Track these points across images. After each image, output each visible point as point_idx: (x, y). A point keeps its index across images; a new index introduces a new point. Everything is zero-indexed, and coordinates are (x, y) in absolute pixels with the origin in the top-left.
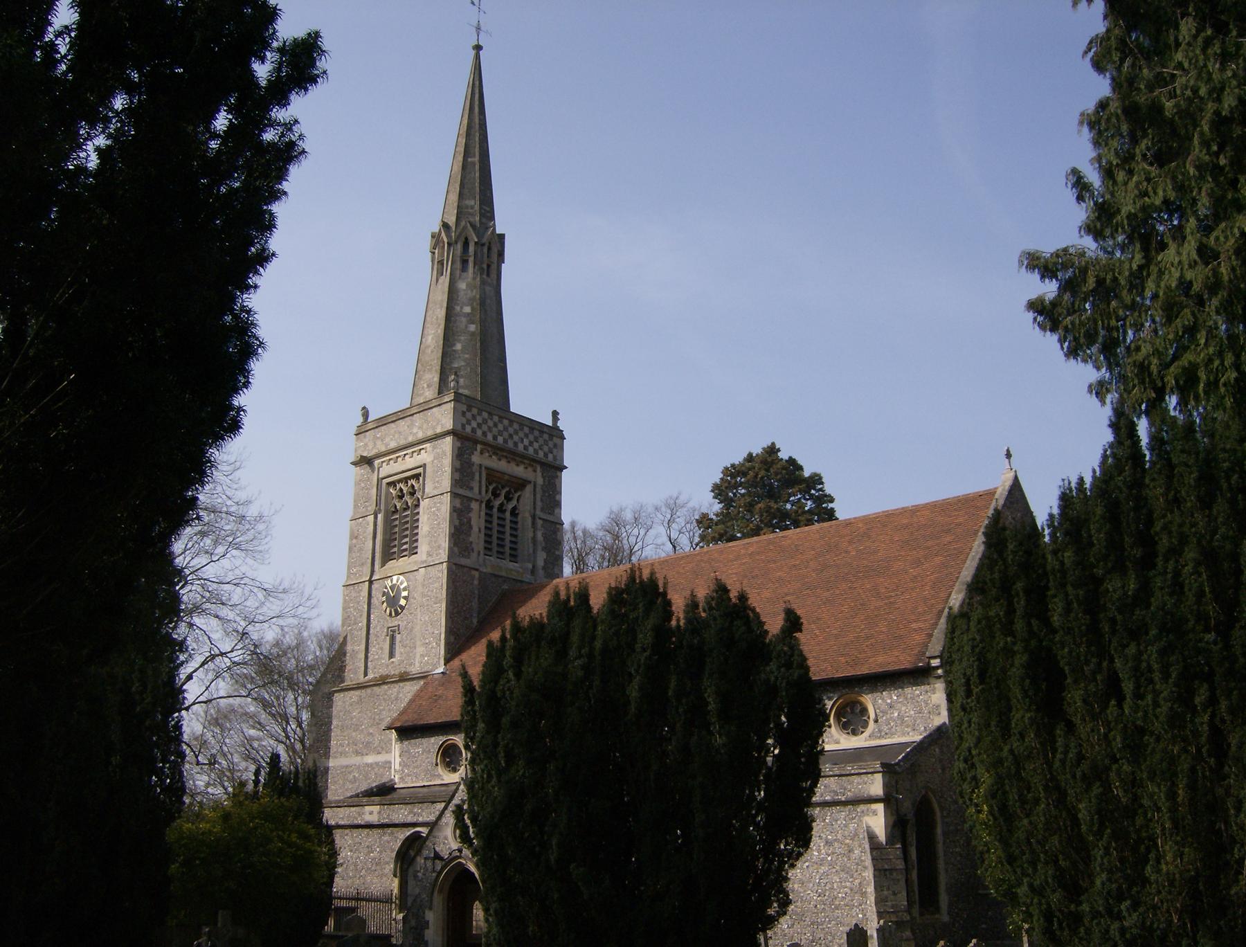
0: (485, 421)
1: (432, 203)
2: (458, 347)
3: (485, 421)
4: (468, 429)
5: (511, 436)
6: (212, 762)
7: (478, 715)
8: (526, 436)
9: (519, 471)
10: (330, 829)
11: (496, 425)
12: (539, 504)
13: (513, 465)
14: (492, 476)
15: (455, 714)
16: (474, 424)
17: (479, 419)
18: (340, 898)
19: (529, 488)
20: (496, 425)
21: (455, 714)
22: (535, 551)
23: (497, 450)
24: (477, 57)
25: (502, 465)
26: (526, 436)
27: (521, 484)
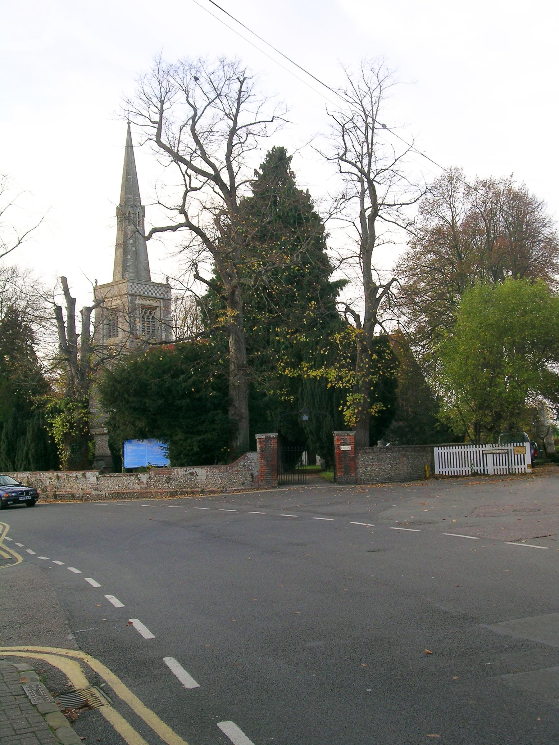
0: (140, 287)
1: (115, 196)
2: (129, 257)
3: (140, 287)
4: (133, 291)
5: (150, 291)
6: (505, 528)
7: (31, 461)
8: (156, 290)
9: (154, 303)
10: (92, 436)
11: (144, 288)
12: (162, 314)
13: (151, 302)
14: (143, 307)
15: (378, 217)
16: (136, 289)
17: (137, 287)
18: (98, 457)
19: (158, 309)
20: (144, 288)
21: (378, 217)
22: (161, 332)
23: (144, 297)
24: (129, 127)
25: (148, 302)
26: (156, 290)
27: (155, 308)
